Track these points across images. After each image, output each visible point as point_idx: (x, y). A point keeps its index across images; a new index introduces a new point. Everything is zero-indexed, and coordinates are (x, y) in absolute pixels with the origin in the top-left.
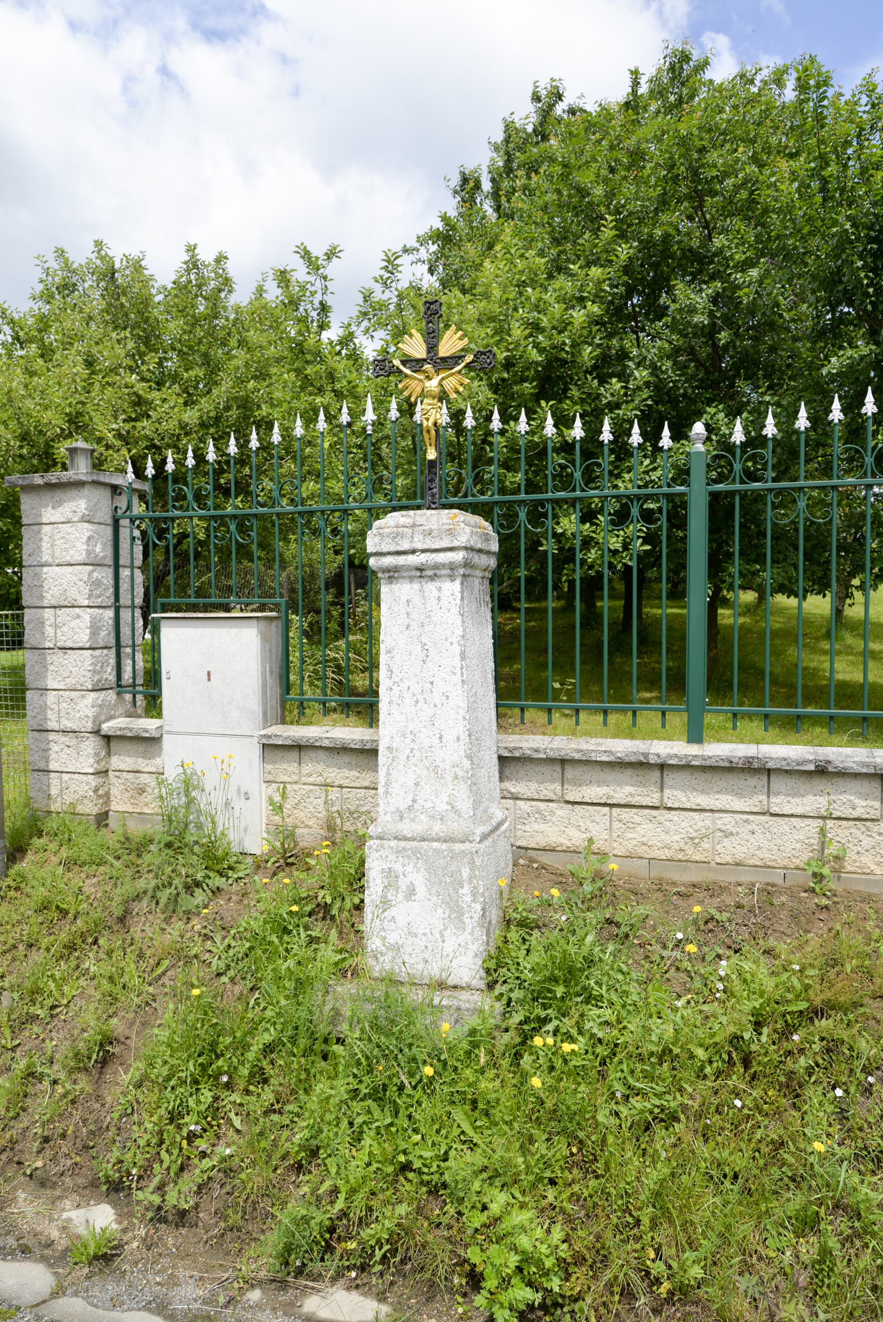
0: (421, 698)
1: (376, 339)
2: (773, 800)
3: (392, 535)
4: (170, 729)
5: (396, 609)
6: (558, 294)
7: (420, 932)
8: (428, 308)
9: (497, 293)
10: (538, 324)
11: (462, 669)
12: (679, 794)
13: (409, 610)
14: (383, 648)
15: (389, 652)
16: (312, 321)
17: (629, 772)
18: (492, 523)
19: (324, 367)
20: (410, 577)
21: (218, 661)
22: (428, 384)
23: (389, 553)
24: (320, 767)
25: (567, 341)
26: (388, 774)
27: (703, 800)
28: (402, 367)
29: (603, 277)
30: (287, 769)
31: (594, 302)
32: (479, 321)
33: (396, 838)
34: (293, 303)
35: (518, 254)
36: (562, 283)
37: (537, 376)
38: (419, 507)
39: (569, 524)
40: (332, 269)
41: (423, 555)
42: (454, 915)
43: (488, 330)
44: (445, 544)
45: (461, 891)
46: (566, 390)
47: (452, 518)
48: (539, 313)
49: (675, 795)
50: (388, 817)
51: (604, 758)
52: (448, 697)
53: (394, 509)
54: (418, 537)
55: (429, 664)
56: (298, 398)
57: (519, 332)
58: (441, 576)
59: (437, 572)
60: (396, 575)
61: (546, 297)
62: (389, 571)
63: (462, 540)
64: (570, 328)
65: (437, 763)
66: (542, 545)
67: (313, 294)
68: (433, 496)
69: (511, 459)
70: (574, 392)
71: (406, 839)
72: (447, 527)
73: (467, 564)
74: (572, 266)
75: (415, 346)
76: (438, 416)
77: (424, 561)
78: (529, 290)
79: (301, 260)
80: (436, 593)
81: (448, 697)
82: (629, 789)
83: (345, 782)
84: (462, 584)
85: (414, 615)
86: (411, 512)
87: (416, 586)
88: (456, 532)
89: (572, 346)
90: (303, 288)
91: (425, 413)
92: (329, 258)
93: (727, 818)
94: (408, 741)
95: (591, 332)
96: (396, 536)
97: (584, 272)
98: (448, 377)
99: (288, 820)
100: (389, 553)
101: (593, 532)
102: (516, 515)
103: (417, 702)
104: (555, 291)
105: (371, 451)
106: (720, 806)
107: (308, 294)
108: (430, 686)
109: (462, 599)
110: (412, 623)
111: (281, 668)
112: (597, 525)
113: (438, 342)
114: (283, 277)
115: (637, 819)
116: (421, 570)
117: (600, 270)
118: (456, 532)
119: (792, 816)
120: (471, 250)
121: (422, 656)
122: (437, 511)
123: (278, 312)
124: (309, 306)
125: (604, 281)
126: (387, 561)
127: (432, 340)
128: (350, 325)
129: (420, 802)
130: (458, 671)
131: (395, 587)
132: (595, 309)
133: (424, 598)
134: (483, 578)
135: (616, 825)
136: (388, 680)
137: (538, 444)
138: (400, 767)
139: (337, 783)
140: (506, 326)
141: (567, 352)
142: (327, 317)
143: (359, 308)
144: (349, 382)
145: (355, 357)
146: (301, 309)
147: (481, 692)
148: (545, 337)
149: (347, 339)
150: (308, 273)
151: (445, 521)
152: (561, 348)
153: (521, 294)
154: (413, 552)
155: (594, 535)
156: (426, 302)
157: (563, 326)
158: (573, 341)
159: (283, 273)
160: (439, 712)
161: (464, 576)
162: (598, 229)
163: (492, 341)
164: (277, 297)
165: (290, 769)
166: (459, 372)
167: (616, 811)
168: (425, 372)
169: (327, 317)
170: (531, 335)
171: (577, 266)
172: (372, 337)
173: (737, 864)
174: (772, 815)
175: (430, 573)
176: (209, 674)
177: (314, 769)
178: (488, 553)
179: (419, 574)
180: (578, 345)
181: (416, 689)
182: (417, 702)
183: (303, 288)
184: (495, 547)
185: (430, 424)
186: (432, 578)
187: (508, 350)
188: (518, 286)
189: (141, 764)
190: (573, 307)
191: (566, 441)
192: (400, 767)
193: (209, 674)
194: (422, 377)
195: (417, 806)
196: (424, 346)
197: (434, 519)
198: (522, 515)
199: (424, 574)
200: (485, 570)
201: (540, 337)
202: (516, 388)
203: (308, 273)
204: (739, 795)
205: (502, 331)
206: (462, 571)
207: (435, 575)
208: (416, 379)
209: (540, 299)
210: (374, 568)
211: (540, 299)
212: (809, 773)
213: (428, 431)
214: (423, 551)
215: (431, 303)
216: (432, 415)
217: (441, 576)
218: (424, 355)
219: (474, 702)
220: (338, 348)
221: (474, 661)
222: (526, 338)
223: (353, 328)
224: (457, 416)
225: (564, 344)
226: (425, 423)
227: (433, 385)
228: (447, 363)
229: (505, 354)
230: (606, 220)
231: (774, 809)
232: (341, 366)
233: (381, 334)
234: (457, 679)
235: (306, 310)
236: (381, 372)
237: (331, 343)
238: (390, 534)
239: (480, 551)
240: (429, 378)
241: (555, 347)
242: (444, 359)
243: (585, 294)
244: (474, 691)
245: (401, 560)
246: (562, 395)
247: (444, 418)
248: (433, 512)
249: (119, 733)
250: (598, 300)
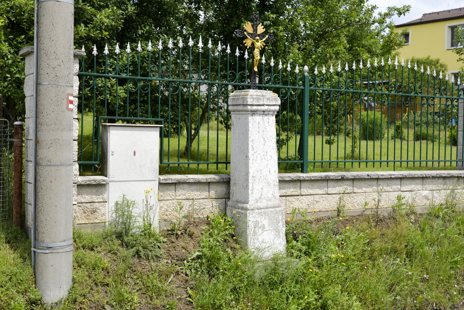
0: (263, 158)
2: (329, 189)
4: (113, 179)
5: (255, 125)
7: (267, 241)
12: (305, 190)
13: (259, 126)
14: (250, 140)
17: (291, 184)
21: (134, 148)
23: (255, 105)
24: (184, 192)
26: (253, 186)
27: (311, 191)
30: (170, 193)
33: (258, 209)
42: (277, 233)
44: (274, 103)
45: (279, 224)
49: (305, 191)
50: (253, 202)
51: (288, 179)
54: (265, 100)
65: (269, 181)
71: (261, 209)
80: (267, 120)
82: (292, 190)
83: (195, 197)
85: (261, 128)
87: (261, 117)
93: (317, 196)
94: (259, 173)
99: (169, 216)
100: (255, 105)
106: (316, 193)
115: (294, 200)
119: (333, 194)
121: (263, 142)
129: (263, 195)
131: (254, 117)
135: (288, 203)
138: (257, 183)
139: (191, 198)
154: (263, 105)
165: (171, 194)
167: (288, 198)
173: (320, 211)
174: (328, 194)
176: (135, 152)
177: (182, 193)
181: (262, 154)
186: (266, 115)
189: (95, 198)
192: (257, 183)
193: (135, 152)
195: (262, 197)
204: (320, 189)
207: (268, 114)
212: (340, 179)
214: (267, 105)
231: (329, 192)
238: (256, 98)
245: (259, 108)
249: (88, 183)
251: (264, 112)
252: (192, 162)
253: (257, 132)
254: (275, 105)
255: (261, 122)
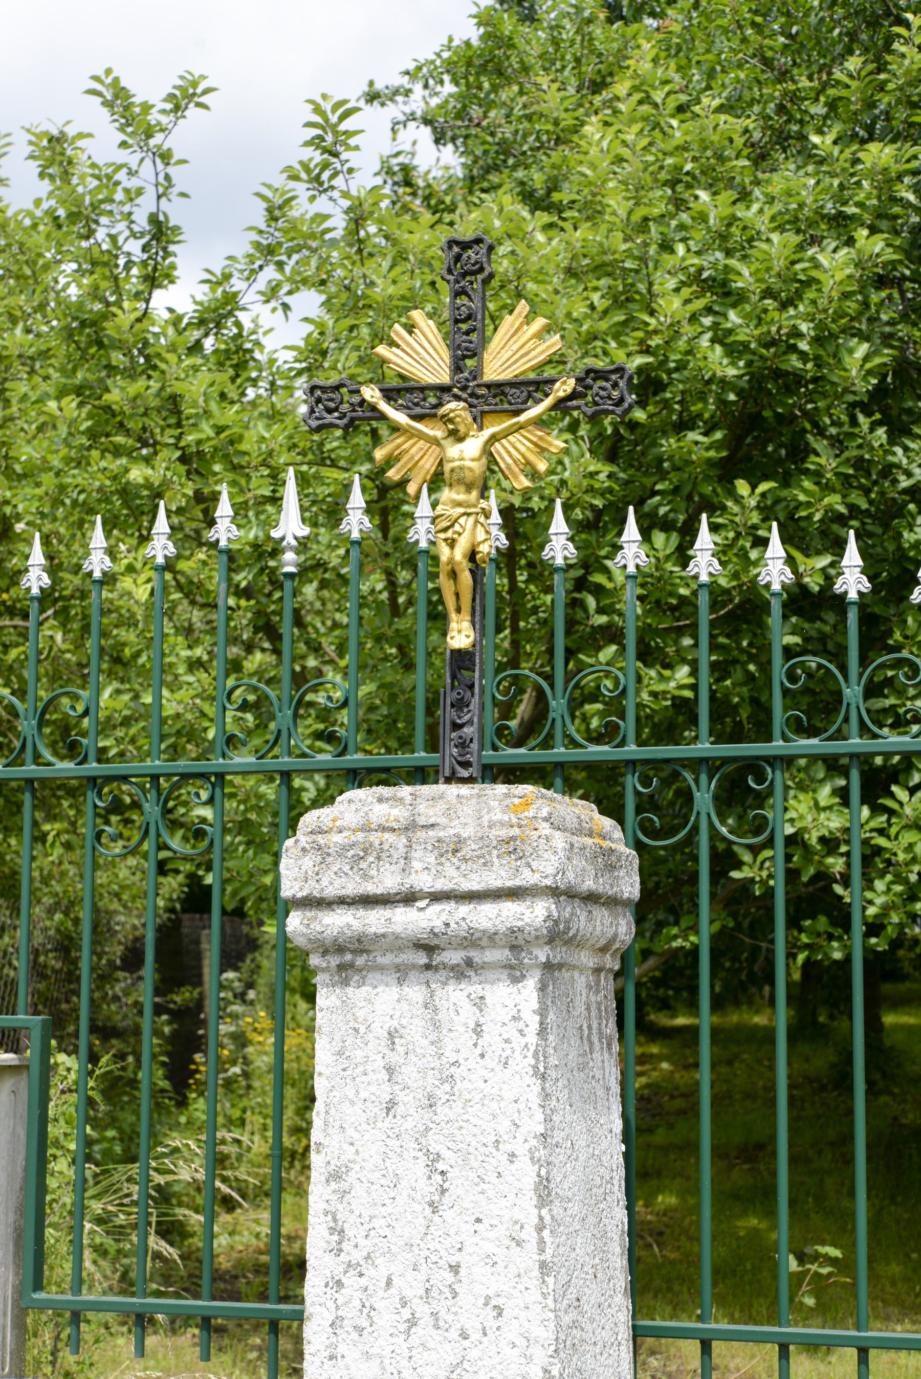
0: (423, 1311)
1: (294, 316)
3: (353, 850)
6: (778, 207)
8: (458, 258)
9: (617, 204)
10: (724, 283)
11: (540, 1228)
13: (395, 1058)
15: (335, 1176)
16: (129, 265)
18: (621, 821)
19: (155, 385)
20: (398, 968)
22: (453, 451)
25: (804, 327)
28: (384, 407)
29: (895, 168)
31: (873, 230)
32: (570, 272)
34: (80, 218)
35: (672, 103)
36: (794, 182)
37: (725, 417)
38: (420, 775)
39: (810, 812)
40: (185, 135)
41: (436, 908)
43: (596, 297)
46: (800, 452)
47: (515, 809)
48: (728, 253)
52: (499, 1311)
53: (358, 777)
54: (422, 858)
55: (448, 1215)
56: (81, 462)
57: (676, 303)
58: (484, 966)
59: (477, 956)
60: (360, 961)
61: (748, 213)
62: (340, 949)
63: (545, 868)
64: (810, 294)
66: (739, 865)
67: (132, 195)
68: (463, 745)
69: (657, 632)
70: (825, 459)
72: (504, 833)
73: (556, 935)
74: (815, 139)
75: (422, 354)
76: (481, 535)
77: (438, 924)
78: (704, 195)
79: (105, 111)
80: (469, 1014)
81: (499, 1311)
84: (543, 988)
85: (409, 1073)
86: (405, 791)
87: (415, 992)
88: (528, 847)
89: (817, 340)
90: (108, 180)
91: (445, 526)
92: (177, 108)
95: (866, 304)
96: (362, 855)
97: (847, 154)
98: (507, 433)
101: (881, 832)
102: (687, 797)
103: (412, 1322)
104: (771, 200)
105: (266, 605)
107: (119, 196)
108: (449, 1277)
109: (543, 1032)
110: (401, 1097)
111: (21, 1211)
112: (891, 812)
113: (484, 341)
114: (55, 154)
116: (430, 949)
117: (889, 150)
118: (528, 847)
120: (554, 96)
121: (427, 1189)
122: (477, 788)
123: (37, 239)
124: (122, 226)
125: (900, 178)
126: (337, 922)
127: (466, 337)
128: (227, 277)
130: (529, 1234)
131: (357, 994)
132: (875, 246)
133: (436, 1025)
134: (597, 971)
136: (329, 1259)
137: (727, 592)
140: (642, 287)
141: (803, 356)
142: (167, 254)
143: (254, 236)
144: (220, 430)
145: (238, 359)
146: (101, 234)
147: (592, 1295)
148: (746, 316)
149: (218, 313)
150: (123, 144)
151: (498, 816)
152: (786, 344)
153: (679, 204)
154: (409, 898)
155: (882, 842)
156: (451, 243)
157: (791, 290)
158: (820, 326)
159: (57, 141)
160: (473, 1354)
161: (549, 967)
162: (888, 48)
163: (604, 325)
164: (38, 202)
166: (539, 422)
168: (446, 419)
169: (167, 254)
170: (709, 310)
171: (829, 139)
172: (286, 307)
175: (454, 957)
178: (612, 902)
179: (422, 959)
180: (833, 336)
181: (410, 1285)
182: (412, 1322)
183: (108, 180)
184: (630, 887)
185: (459, 554)
186: (460, 972)
187: (647, 351)
188: (673, 183)
190: (815, 241)
191: (803, 588)
194: (439, 433)
196: (446, 354)
197: (467, 810)
198: (704, 798)
199: (437, 959)
200: (604, 950)
201: (732, 315)
202: (668, 444)
203: (123, 144)
205: (631, 299)
206: (542, 954)
208: (421, 436)
209: (733, 220)
210: (300, 942)
211: (733, 220)
213: (453, 574)
214: (436, 897)
215: (465, 246)
216: (458, 530)
217: (484, 966)
218: (444, 377)
219: (575, 1325)
220: (196, 334)
221: (574, 1208)
222: (693, 318)
223: (237, 284)
224: (522, 524)
225: (796, 333)
226: (444, 553)
227: (467, 453)
228: (507, 396)
229: (640, 360)
230: (907, 25)
232: (197, 385)
233: (309, 302)
234: (528, 1258)
235: (113, 238)
236: (329, 418)
237: (176, 321)
238: (345, 848)
239: (591, 898)
240: (457, 436)
241: (773, 343)
242: (498, 388)
243: (851, 210)
244: (572, 1294)
245: (374, 921)
246: (792, 462)
247: (491, 538)
248: (465, 790)
250: (884, 224)
251: (428, 948)
252: (724, 1326)
253: (377, 1110)
254: (514, 894)
255: (416, 1031)
